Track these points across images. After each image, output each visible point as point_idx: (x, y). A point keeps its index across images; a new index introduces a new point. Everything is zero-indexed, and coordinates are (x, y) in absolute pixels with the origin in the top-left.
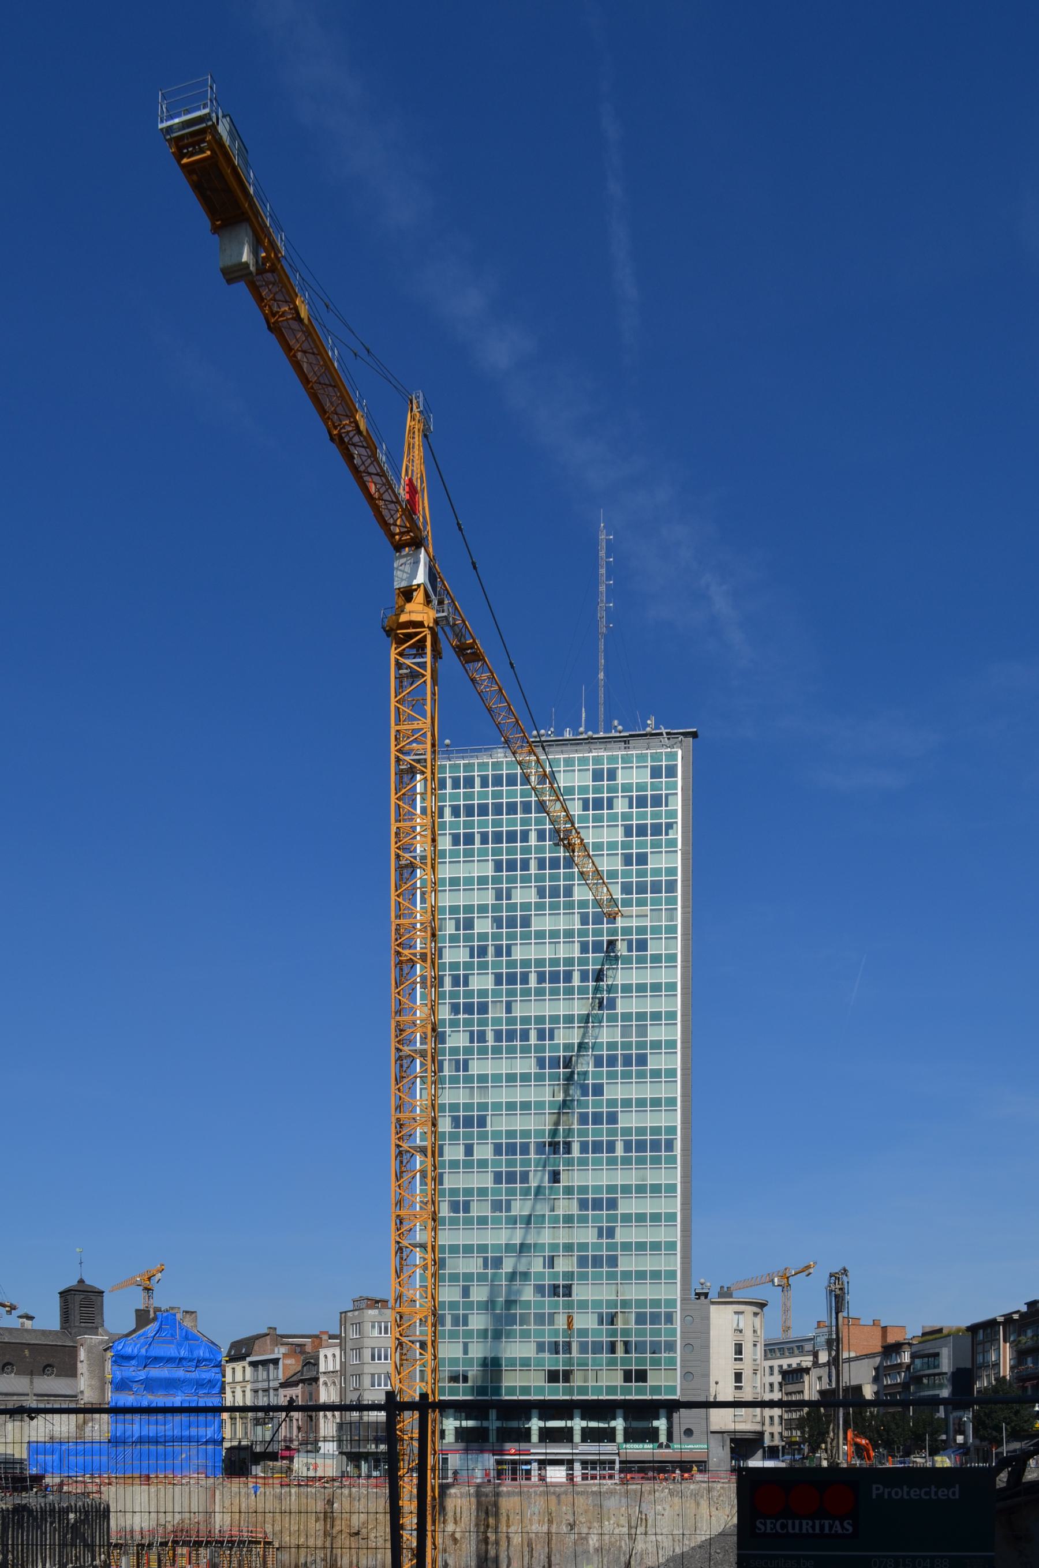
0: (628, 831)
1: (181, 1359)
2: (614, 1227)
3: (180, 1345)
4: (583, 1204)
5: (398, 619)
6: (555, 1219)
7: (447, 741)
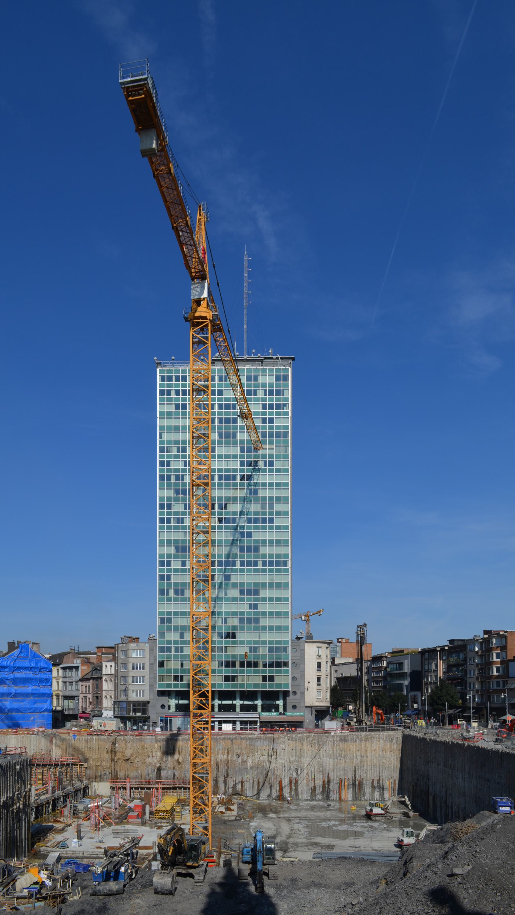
0: (264, 407)
1: (31, 668)
2: (257, 604)
3: (30, 660)
4: (242, 592)
5: (194, 315)
6: (228, 599)
7: (173, 358)
